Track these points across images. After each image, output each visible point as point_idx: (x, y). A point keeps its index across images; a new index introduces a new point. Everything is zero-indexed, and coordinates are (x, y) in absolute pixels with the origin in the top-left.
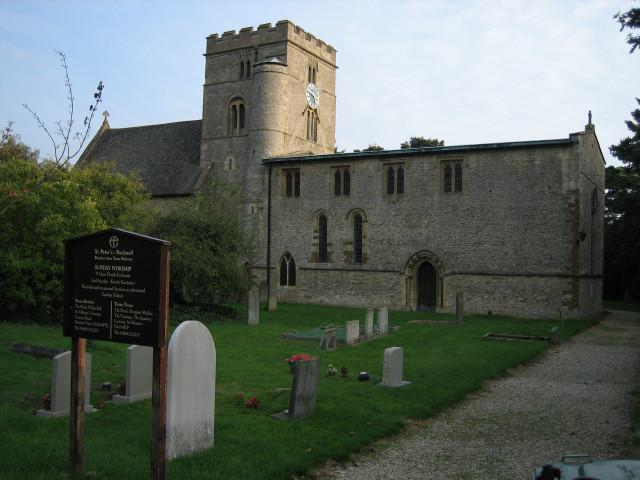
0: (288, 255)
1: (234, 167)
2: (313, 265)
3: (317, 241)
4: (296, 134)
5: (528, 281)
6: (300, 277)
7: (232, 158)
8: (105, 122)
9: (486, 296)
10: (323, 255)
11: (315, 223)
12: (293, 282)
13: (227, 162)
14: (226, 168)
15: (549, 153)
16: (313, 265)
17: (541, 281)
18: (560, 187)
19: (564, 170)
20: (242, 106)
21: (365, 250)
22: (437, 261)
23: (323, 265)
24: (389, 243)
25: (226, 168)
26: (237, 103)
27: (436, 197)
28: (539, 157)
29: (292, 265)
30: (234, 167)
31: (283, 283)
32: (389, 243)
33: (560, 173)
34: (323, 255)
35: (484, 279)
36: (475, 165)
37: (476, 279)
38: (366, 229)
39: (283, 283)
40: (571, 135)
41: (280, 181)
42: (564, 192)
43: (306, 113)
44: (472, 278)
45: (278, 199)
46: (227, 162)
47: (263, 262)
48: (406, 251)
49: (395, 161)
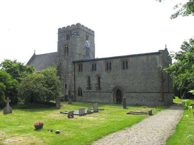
0: (80, 88)
1: (66, 64)
2: (87, 91)
3: (88, 84)
4: (83, 54)
5: (149, 94)
6: (84, 94)
7: (65, 61)
8: (35, 53)
9: (136, 99)
10: (89, 88)
11: (87, 79)
12: (81, 96)
13: (64, 63)
14: (64, 64)
15: (153, 56)
16: (77, 89)
17: (152, 94)
18: (157, 66)
19: (158, 61)
20: (67, 47)
21: (101, 86)
22: (121, 89)
23: (89, 91)
24: (108, 84)
25: (64, 64)
26: (66, 46)
27: (121, 70)
28: (150, 57)
29: (81, 91)
30: (66, 64)
31: (79, 96)
32: (108, 84)
33: (156, 62)
34: (89, 88)
35: (135, 94)
36: (132, 61)
37: (133, 94)
38: (101, 80)
39: (79, 96)
40: (159, 51)
41: (77, 67)
42: (158, 68)
43: (86, 48)
44: (132, 94)
45: (77, 73)
46: (64, 63)
47: (73, 90)
48: (113, 86)
49: (108, 60)
